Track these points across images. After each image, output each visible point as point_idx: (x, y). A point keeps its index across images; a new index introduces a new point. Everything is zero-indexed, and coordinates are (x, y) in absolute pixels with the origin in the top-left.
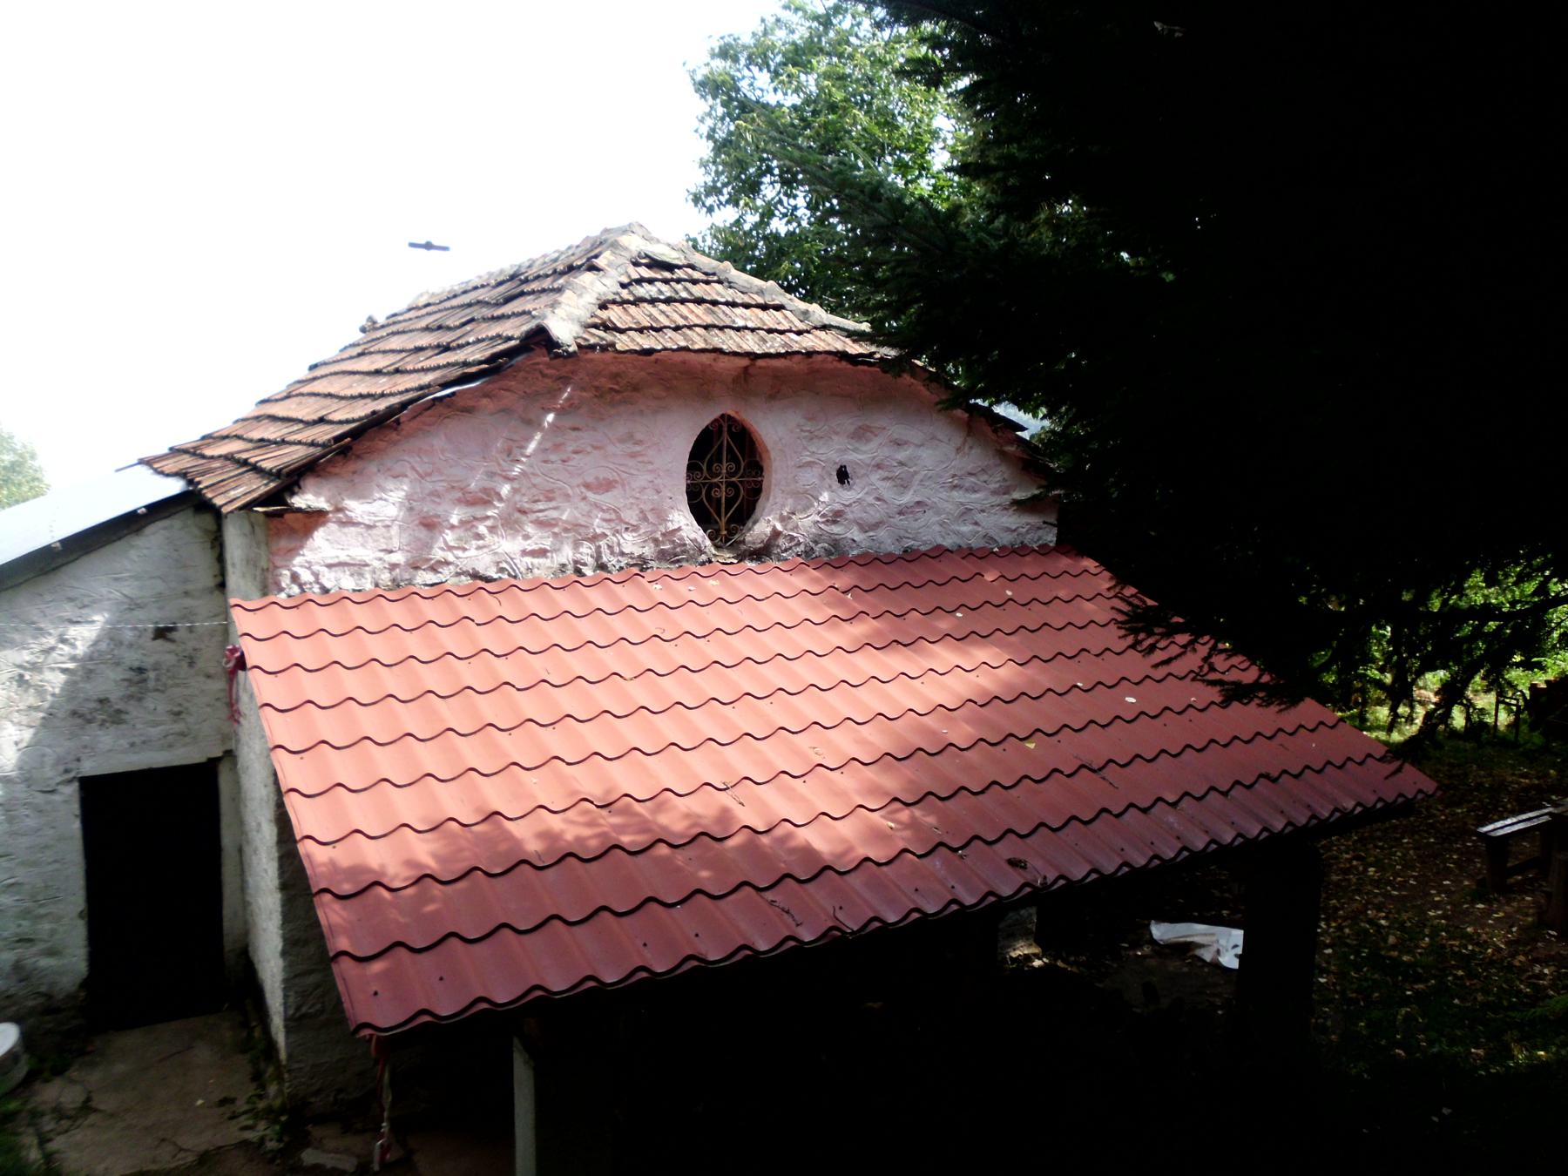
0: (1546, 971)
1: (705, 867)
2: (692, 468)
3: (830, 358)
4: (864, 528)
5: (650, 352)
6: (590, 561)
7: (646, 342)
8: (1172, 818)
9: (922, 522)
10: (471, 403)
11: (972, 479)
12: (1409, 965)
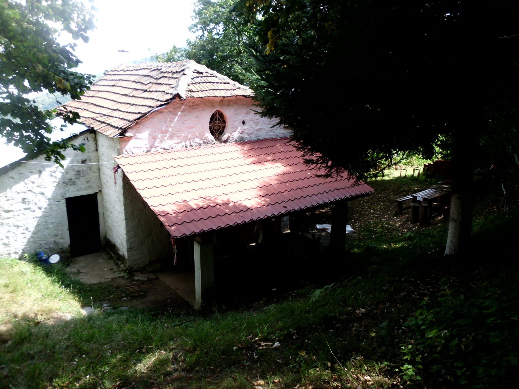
1: (227, 210)
2: (210, 122)
4: (248, 135)
6: (189, 145)
7: (201, 95)
8: (316, 198)
9: (262, 132)
12: (375, 231)
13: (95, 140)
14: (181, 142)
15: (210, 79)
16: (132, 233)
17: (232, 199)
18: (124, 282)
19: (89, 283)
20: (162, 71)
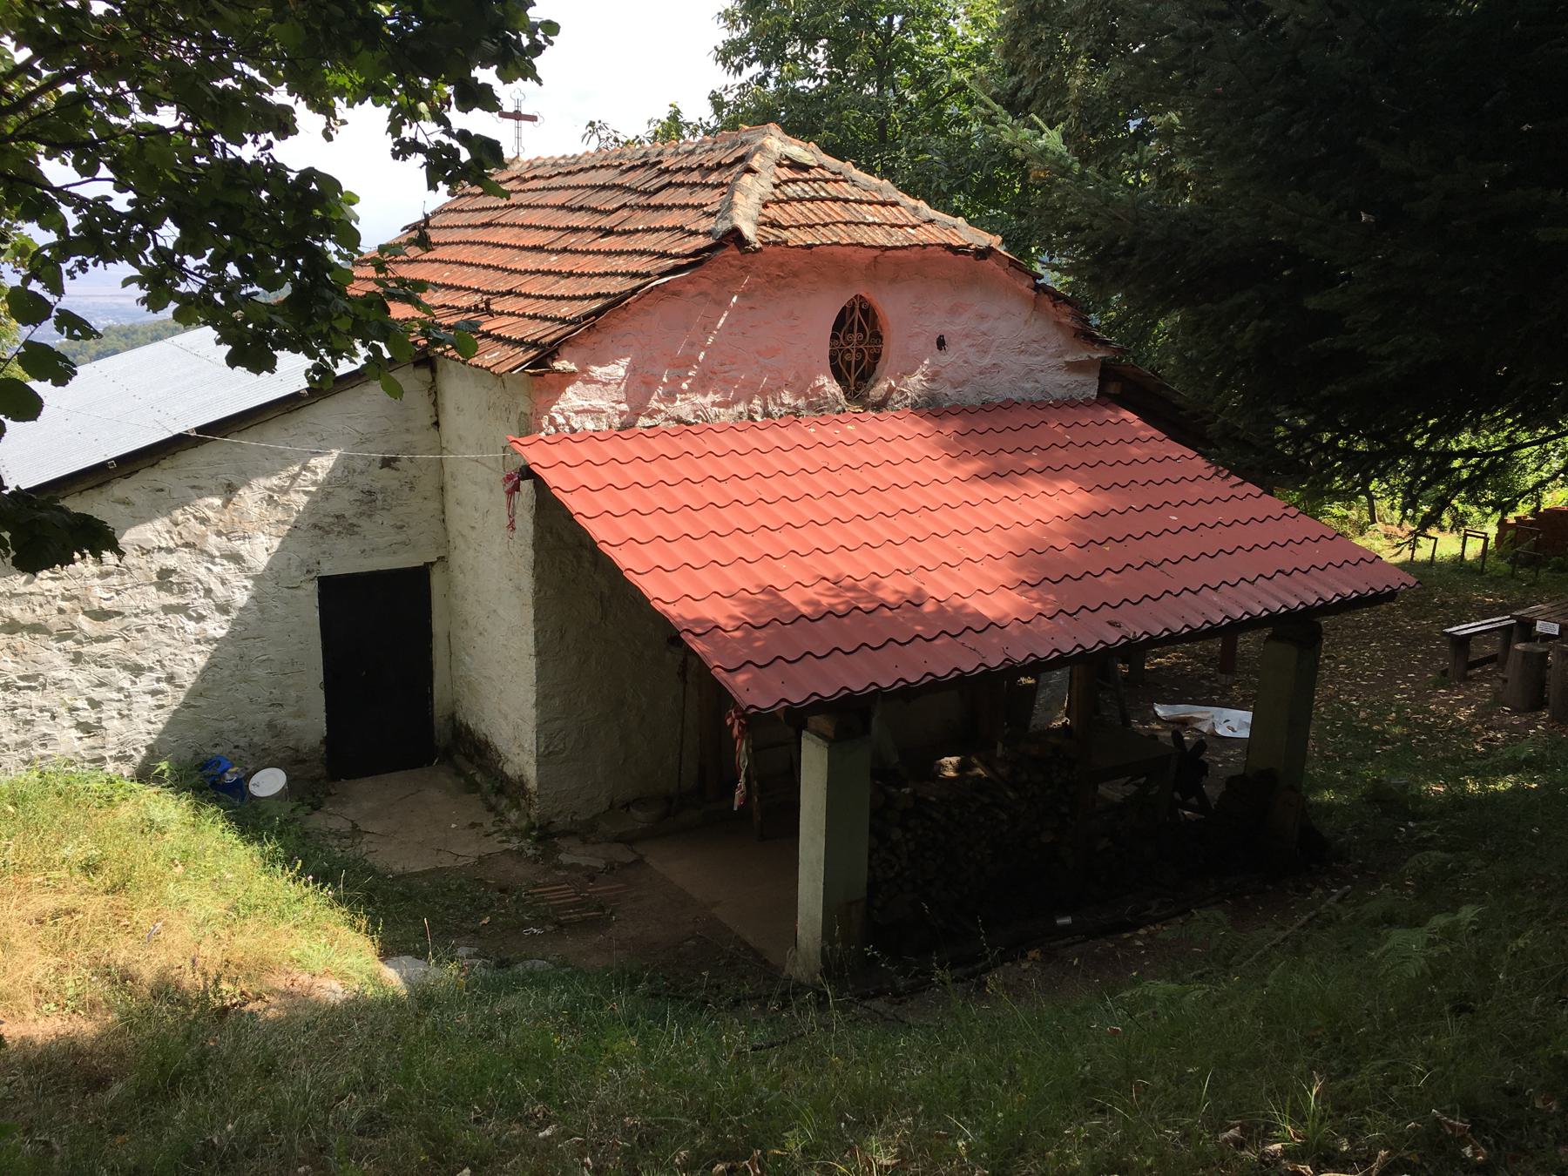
0: (1499, 736)
2: (834, 337)
3: (939, 249)
5: (810, 247)
6: (760, 410)
10: (679, 288)
11: (1035, 345)
12: (1378, 732)
13: (434, 391)
14: (736, 402)
15: (832, 189)
16: (557, 701)
17: (929, 590)
18: (521, 871)
19: (398, 868)
20: (663, 166)
